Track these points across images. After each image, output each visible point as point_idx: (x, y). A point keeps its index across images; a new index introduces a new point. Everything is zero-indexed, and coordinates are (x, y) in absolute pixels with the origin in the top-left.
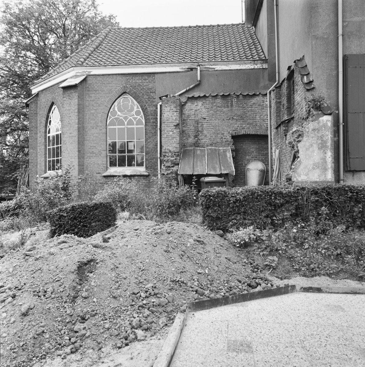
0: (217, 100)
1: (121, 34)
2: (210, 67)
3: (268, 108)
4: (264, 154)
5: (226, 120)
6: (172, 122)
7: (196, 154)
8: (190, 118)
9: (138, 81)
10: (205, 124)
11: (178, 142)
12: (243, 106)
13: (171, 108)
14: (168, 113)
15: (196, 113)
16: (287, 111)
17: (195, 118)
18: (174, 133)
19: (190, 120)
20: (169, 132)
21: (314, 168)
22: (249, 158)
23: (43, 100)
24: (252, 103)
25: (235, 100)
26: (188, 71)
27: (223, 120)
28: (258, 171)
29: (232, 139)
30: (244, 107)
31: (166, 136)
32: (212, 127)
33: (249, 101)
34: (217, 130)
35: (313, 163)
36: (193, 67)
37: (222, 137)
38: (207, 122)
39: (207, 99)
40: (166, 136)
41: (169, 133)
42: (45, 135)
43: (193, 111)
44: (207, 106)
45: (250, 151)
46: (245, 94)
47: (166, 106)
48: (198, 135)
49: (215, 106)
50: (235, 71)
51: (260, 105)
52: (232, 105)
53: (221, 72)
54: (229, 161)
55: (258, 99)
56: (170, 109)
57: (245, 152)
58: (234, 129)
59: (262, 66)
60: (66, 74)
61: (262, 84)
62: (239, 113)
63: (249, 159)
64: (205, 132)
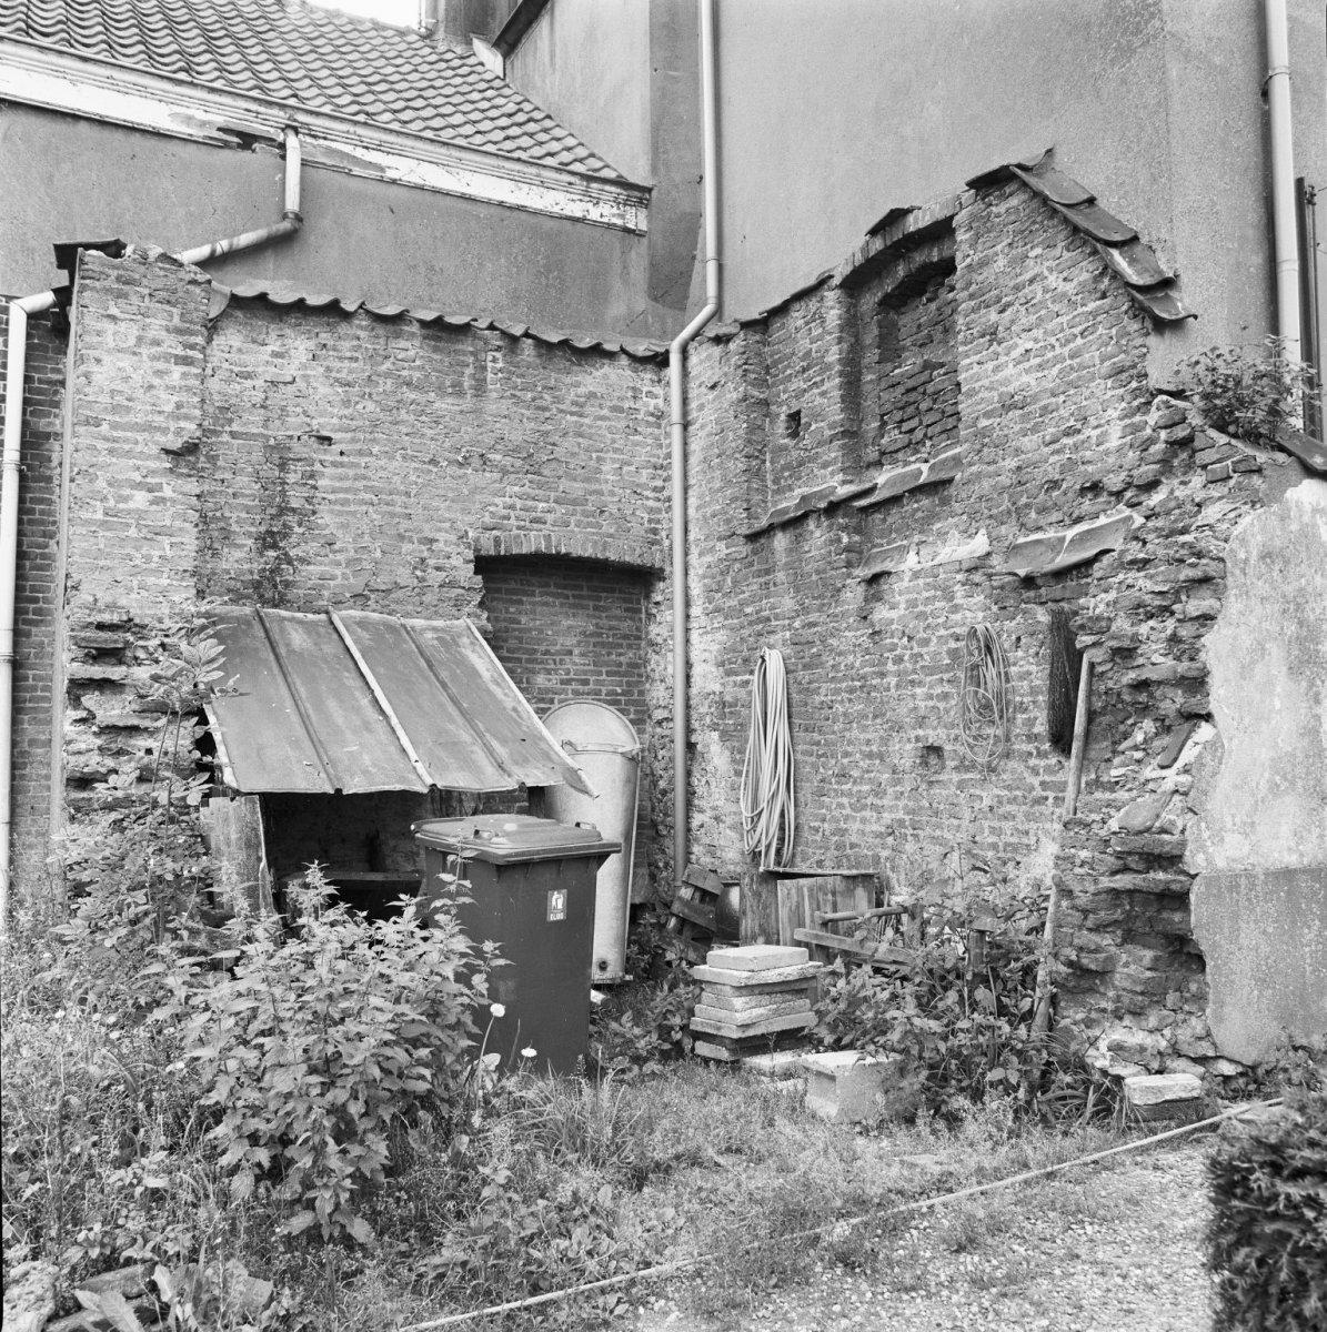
0: (402, 344)
2: (359, 153)
3: (676, 431)
4: (620, 665)
5: (450, 462)
6: (149, 428)
7: (291, 652)
8: (235, 427)
10: (329, 471)
11: (189, 565)
12: (539, 403)
13: (151, 334)
14: (126, 362)
15: (276, 399)
16: (843, 447)
17: (265, 426)
18: (163, 500)
19: (233, 435)
20: (126, 492)
21: (1278, 786)
22: (549, 685)
24: (582, 390)
25: (494, 360)
26: (226, 145)
27: (433, 462)
28: (619, 760)
29: (476, 573)
30: (545, 409)
31: (99, 516)
32: (368, 496)
33: (568, 380)
34: (393, 515)
35: (1273, 760)
36: (256, 127)
37: (423, 560)
38: (342, 465)
39: (343, 328)
40: (99, 516)
41: (126, 499)
43: (259, 383)
44: (344, 370)
46: (554, 338)
47: (114, 311)
48: (286, 536)
49: (388, 375)
50: (493, 210)
51: (621, 410)
52: (480, 388)
53: (418, 195)
54: (509, 704)
55: (613, 377)
56: (140, 339)
57: (527, 651)
58: (487, 519)
59: (622, 217)
61: (617, 309)
62: (516, 437)
63: (547, 691)
64: (326, 519)
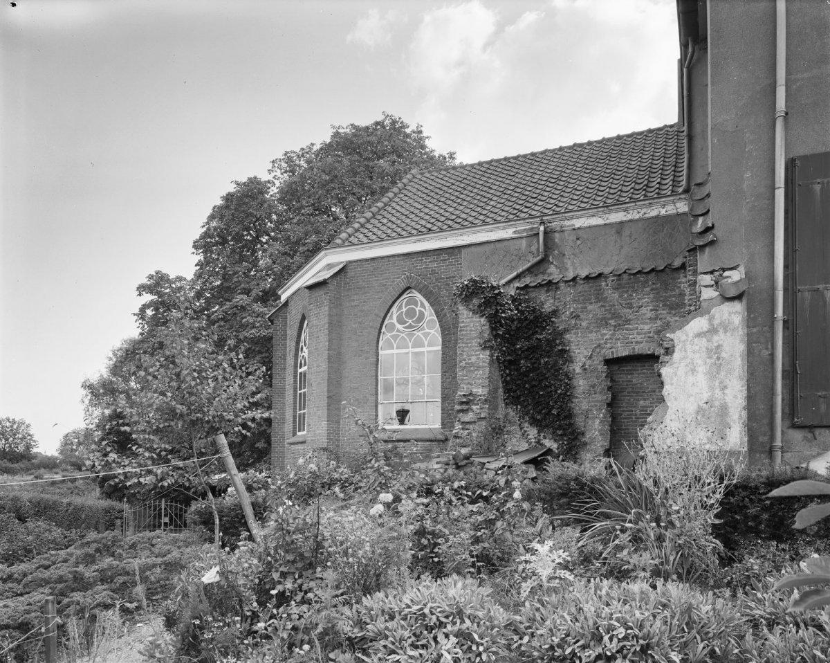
1: (543, 183)
9: (421, 265)
22: (645, 404)
23: (294, 312)
42: (294, 371)
45: (647, 391)
60: (320, 260)
63: (644, 407)
